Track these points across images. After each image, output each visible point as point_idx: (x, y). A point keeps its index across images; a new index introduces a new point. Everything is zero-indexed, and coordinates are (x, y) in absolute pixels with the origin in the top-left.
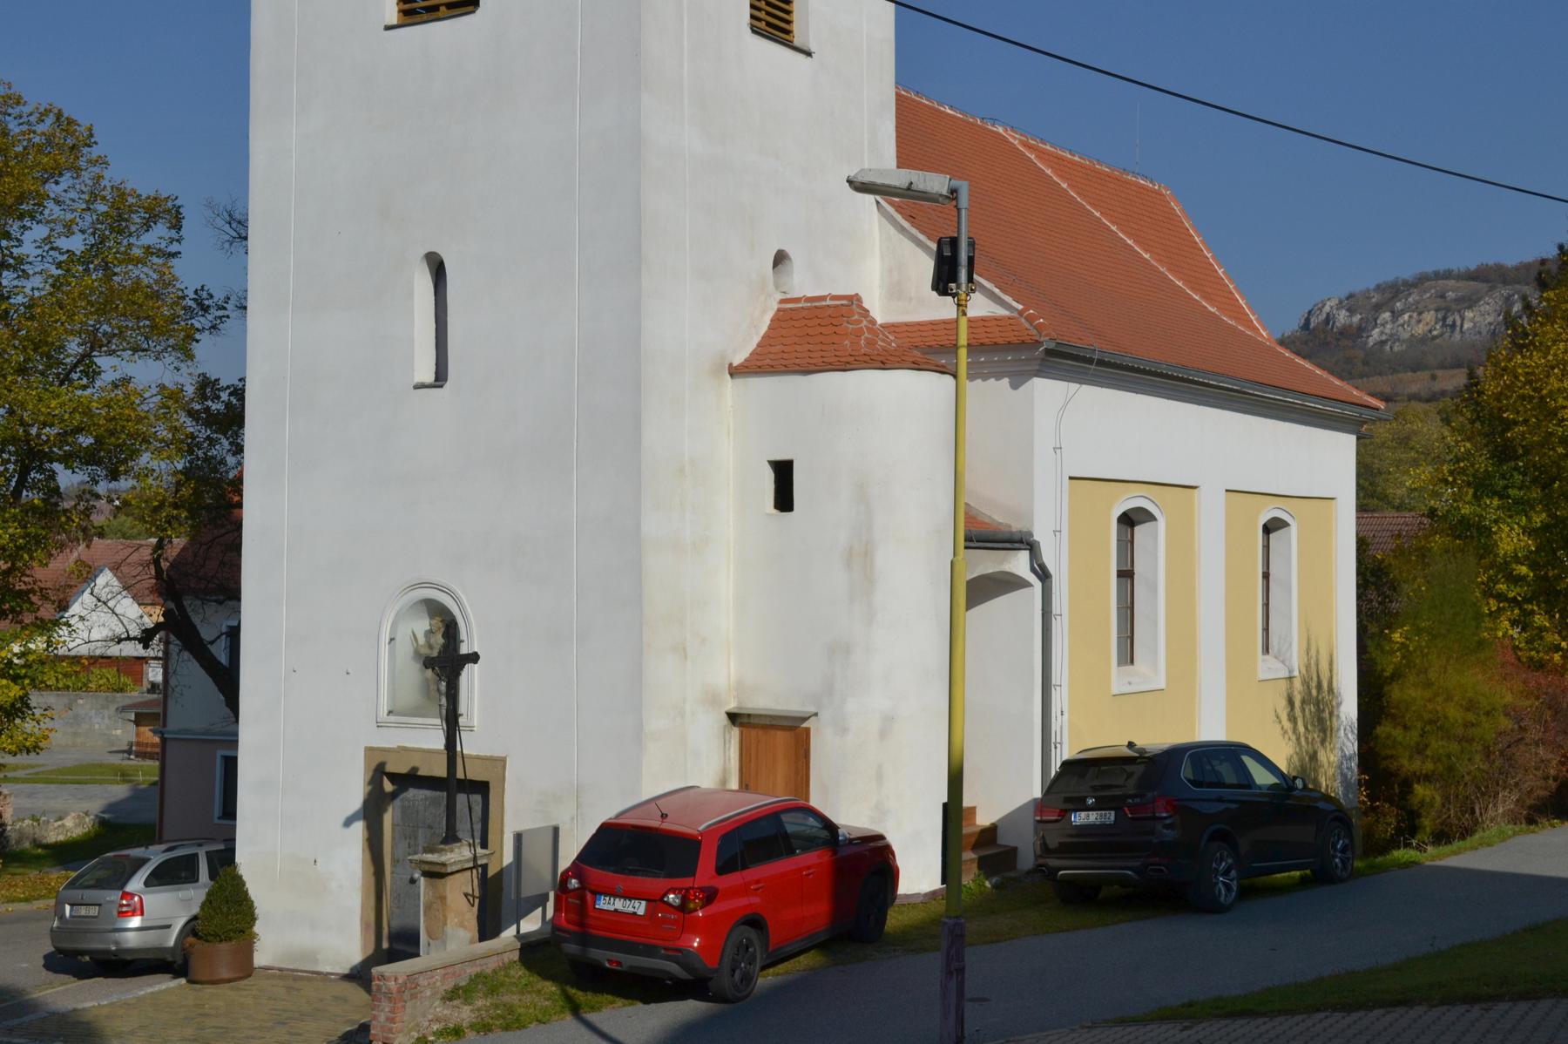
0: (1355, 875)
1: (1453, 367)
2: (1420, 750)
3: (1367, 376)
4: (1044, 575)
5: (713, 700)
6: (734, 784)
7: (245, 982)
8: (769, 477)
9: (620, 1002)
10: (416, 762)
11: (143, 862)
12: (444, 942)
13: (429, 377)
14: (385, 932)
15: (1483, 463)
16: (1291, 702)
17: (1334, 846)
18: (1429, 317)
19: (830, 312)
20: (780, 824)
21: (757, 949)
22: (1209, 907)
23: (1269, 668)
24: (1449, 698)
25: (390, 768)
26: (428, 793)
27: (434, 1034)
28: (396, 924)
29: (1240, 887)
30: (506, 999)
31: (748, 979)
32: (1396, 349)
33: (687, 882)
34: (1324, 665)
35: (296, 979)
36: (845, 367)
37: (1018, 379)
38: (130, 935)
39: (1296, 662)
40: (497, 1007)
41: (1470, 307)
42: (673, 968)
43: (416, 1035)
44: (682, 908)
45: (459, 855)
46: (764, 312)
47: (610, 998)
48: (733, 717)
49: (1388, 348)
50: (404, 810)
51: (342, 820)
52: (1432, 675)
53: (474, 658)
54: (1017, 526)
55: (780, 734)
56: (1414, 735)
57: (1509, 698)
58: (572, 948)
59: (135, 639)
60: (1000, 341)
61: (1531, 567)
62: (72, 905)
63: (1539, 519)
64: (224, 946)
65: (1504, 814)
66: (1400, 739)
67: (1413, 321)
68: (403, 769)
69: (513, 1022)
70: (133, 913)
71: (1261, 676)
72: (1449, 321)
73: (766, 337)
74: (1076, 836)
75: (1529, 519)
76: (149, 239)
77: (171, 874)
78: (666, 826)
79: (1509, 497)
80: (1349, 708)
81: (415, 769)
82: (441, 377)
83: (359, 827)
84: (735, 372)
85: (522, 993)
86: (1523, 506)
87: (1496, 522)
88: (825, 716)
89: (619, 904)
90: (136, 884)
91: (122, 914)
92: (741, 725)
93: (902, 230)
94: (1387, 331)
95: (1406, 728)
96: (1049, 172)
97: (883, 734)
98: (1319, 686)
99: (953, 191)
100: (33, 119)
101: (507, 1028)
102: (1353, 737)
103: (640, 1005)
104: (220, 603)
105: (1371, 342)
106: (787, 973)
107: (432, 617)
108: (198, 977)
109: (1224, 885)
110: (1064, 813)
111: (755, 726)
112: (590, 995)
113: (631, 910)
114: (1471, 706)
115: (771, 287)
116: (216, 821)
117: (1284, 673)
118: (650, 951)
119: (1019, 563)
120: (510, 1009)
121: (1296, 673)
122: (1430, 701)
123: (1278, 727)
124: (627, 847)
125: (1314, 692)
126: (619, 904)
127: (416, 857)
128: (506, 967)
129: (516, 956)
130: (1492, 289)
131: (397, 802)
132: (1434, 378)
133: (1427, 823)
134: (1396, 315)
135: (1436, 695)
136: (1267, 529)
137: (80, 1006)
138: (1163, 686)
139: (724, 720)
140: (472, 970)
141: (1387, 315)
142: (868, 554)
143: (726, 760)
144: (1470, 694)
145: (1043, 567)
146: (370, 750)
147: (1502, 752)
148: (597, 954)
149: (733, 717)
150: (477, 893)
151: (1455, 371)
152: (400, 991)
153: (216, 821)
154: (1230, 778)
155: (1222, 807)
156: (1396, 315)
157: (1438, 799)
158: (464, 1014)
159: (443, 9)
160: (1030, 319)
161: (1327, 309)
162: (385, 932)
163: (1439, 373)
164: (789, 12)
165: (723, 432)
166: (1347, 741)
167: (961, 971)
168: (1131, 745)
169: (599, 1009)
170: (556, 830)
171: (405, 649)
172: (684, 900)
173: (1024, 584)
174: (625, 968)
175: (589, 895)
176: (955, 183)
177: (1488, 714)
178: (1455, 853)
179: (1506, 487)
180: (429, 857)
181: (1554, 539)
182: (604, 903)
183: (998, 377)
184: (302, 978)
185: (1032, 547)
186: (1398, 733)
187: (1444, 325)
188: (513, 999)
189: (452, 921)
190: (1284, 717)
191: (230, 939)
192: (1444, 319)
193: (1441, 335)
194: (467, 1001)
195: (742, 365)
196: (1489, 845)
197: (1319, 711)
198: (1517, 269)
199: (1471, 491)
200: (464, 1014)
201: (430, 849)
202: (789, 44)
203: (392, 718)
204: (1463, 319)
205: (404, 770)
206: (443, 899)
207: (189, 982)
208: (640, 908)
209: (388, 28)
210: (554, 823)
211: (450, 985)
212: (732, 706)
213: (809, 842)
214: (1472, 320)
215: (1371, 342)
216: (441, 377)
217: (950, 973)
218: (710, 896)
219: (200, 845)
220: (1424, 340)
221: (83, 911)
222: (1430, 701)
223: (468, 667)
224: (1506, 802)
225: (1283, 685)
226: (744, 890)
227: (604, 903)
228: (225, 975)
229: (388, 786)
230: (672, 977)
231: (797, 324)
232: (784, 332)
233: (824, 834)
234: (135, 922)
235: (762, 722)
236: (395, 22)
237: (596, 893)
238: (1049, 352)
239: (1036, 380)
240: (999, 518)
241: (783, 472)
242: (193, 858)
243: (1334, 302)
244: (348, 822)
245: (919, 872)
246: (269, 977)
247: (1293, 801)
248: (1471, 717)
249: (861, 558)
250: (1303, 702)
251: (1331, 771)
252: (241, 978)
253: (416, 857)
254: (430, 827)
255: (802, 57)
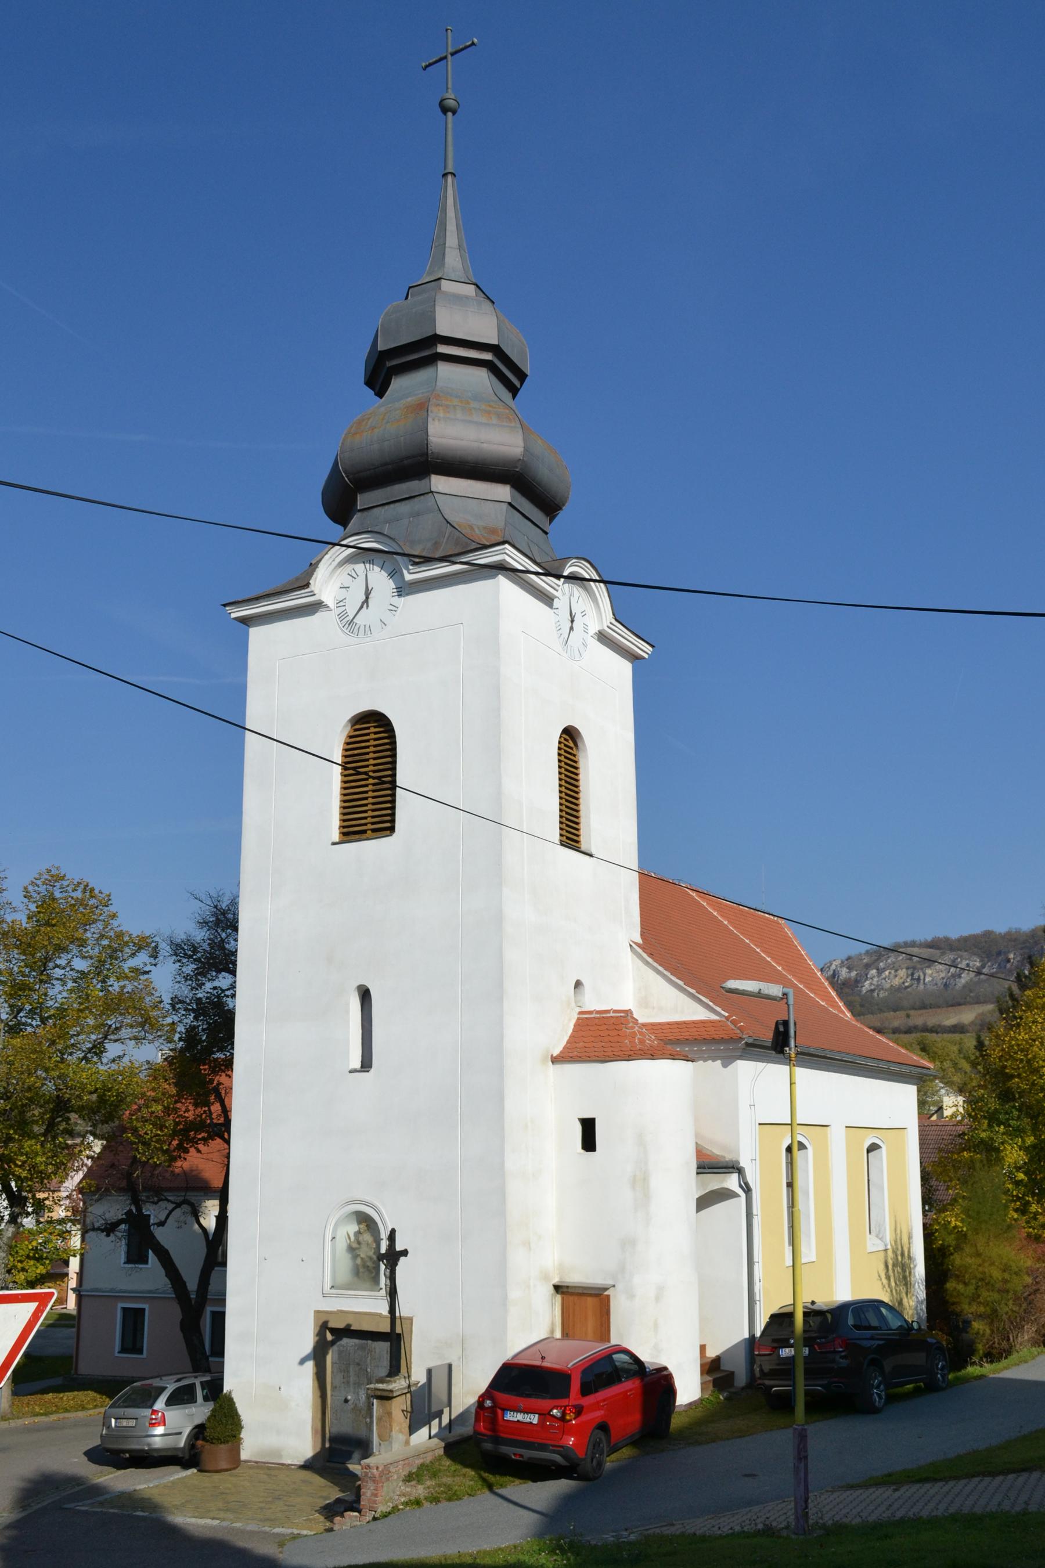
0: (950, 1385)
1: (920, 1009)
2: (975, 1298)
3: (864, 1014)
4: (747, 1190)
5: (546, 1277)
6: (558, 1334)
7: (236, 1471)
8: (578, 1129)
9: (517, 1481)
10: (350, 1320)
11: (163, 1389)
12: (391, 1443)
13: (357, 1065)
14: (327, 1436)
15: (993, 1104)
16: (887, 1266)
17: (937, 1365)
18: (902, 973)
19: (613, 1021)
20: (612, 1361)
21: (604, 1445)
22: (869, 1410)
23: (874, 1244)
24: (992, 1264)
25: (331, 1325)
26: (357, 1341)
27: (403, 1504)
28: (335, 1430)
29: (887, 1395)
30: (445, 1480)
31: (600, 1464)
32: (881, 995)
33: (564, 1402)
34: (905, 1240)
35: (269, 1468)
36: (629, 1058)
37: (727, 1061)
38: (157, 1439)
39: (889, 1237)
40: (440, 1486)
41: (929, 967)
42: (558, 1458)
43: (391, 1505)
44: (562, 1419)
45: (398, 1384)
46: (570, 1020)
47: (511, 1479)
48: (557, 1288)
49: (875, 994)
50: (340, 1353)
51: (298, 1360)
52: (981, 1249)
53: (405, 1253)
54: (729, 1157)
55: (589, 1299)
56: (971, 1289)
57: (1029, 1263)
58: (488, 1446)
59: (98, 1229)
60: (707, 1037)
61: (1025, 1174)
62: (116, 1419)
63: (1030, 1140)
64: (222, 1446)
65: (1029, 1341)
66: (962, 1291)
67: (892, 976)
68: (341, 1325)
69: (453, 1496)
70: (159, 1424)
71: (870, 1249)
72: (916, 976)
73: (572, 1036)
74: (784, 1364)
75: (1023, 1141)
76: (132, 963)
77: (181, 1397)
78: (546, 1364)
79: (1010, 1126)
80: (920, 1270)
81: (349, 1325)
82: (366, 1064)
83: (310, 1365)
84: (555, 1060)
85: (454, 1476)
86: (1018, 1132)
87: (1002, 1143)
88: (620, 1286)
89: (520, 1417)
90: (160, 1404)
91: (153, 1425)
92: (563, 1293)
93: (647, 963)
94: (875, 982)
95: (966, 1284)
96: (715, 914)
97: (658, 1299)
98: (903, 1255)
99: (785, 994)
100: (70, 889)
101: (450, 1500)
102: (923, 1287)
103: (531, 1483)
104: (156, 1203)
105: (864, 990)
106: (618, 1460)
107: (359, 1223)
108: (207, 1468)
109: (877, 1394)
110: (775, 1349)
111: (572, 1294)
112: (498, 1477)
113: (528, 1420)
114: (1006, 1269)
115: (573, 1004)
116: (117, 1355)
117: (882, 1248)
118: (543, 1447)
119: (732, 1182)
120: (449, 1487)
121: (889, 1247)
122: (980, 1265)
123: (880, 1283)
124: (517, 1379)
125: (900, 1258)
126: (520, 1417)
127: (372, 1386)
128: (439, 1459)
129: (441, 1452)
130: (943, 954)
131: (335, 1347)
132: (908, 1016)
133: (980, 1348)
134: (880, 972)
135: (984, 1261)
136: (868, 1151)
137: (138, 1488)
138: (814, 1259)
139: (552, 1290)
140: (419, 1462)
141: (874, 972)
142: (646, 1180)
143: (553, 1316)
144: (1004, 1261)
145: (747, 1184)
146: (317, 1313)
147: (1025, 1299)
148: (505, 1449)
149: (557, 1288)
150: (409, 1409)
151: (924, 1011)
152: (381, 1476)
153: (117, 1355)
154: (874, 1322)
155: (872, 1342)
156: (880, 972)
157: (988, 1331)
158: (420, 1491)
159: (369, 832)
160: (733, 1022)
161: (833, 967)
162: (327, 1436)
163: (912, 1012)
164: (578, 830)
165: (548, 1098)
166: (920, 1291)
167: (806, 1457)
168: (813, 1303)
169: (505, 1486)
170: (450, 1366)
171: (342, 1244)
172: (564, 1414)
173: (735, 1195)
174: (525, 1458)
175: (499, 1411)
176: (786, 990)
177: (1016, 1273)
178: (1006, 1368)
179: (1008, 1120)
180: (380, 1386)
181: (1039, 1153)
182: (511, 1416)
183: (714, 1059)
184: (274, 1468)
185: (740, 1171)
186: (960, 1287)
187: (912, 979)
188: (448, 1480)
189: (396, 1428)
190: (883, 1276)
191: (228, 1442)
192: (912, 974)
193: (911, 985)
194: (419, 1482)
195: (558, 1056)
196: (1026, 1362)
197: (904, 1271)
198: (959, 940)
199: (986, 1122)
200: (420, 1491)
201: (381, 1381)
202: (578, 850)
203: (334, 1291)
204: (925, 975)
205: (341, 1325)
206: (390, 1414)
207: (199, 1471)
208: (535, 1419)
209: (334, 844)
210: (448, 1362)
211: (406, 1473)
212: (556, 1280)
213: (629, 1374)
214: (931, 976)
215: (864, 990)
216: (366, 1064)
217: (800, 1459)
218: (579, 1411)
219: (196, 1377)
220: (899, 989)
221: (124, 1423)
222: (980, 1265)
223: (402, 1259)
224: (1029, 1332)
225: (882, 1254)
226: (596, 1406)
227: (511, 1416)
228: (225, 1467)
229: (329, 1337)
230: (553, 1462)
231: (592, 1028)
232: (583, 1034)
233: (635, 1367)
234: (160, 1430)
235: (577, 1291)
236: (337, 840)
237: (504, 1410)
238: (748, 1045)
239: (739, 1061)
240: (717, 1152)
241: (588, 1127)
242: (191, 1388)
243: (838, 962)
244: (302, 1362)
245: (688, 1389)
246: (251, 1468)
247: (905, 1338)
248: (1006, 1276)
249: (641, 1182)
250: (894, 1265)
251: (911, 1312)
252: (234, 1468)
253: (372, 1386)
254: (358, 1364)
255: (587, 857)
